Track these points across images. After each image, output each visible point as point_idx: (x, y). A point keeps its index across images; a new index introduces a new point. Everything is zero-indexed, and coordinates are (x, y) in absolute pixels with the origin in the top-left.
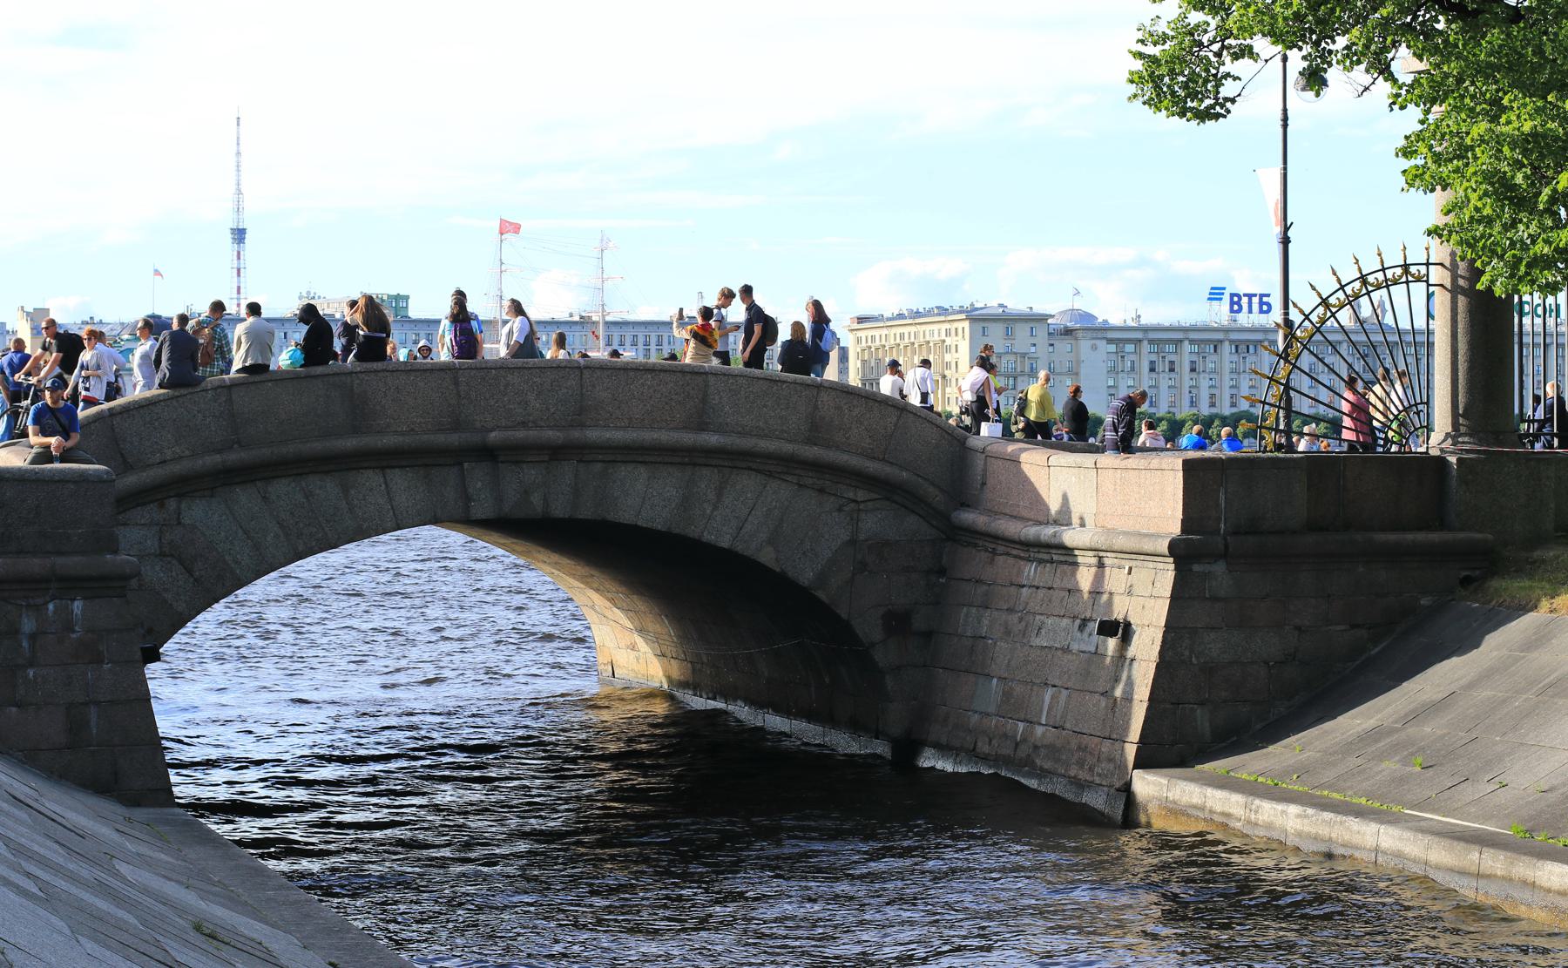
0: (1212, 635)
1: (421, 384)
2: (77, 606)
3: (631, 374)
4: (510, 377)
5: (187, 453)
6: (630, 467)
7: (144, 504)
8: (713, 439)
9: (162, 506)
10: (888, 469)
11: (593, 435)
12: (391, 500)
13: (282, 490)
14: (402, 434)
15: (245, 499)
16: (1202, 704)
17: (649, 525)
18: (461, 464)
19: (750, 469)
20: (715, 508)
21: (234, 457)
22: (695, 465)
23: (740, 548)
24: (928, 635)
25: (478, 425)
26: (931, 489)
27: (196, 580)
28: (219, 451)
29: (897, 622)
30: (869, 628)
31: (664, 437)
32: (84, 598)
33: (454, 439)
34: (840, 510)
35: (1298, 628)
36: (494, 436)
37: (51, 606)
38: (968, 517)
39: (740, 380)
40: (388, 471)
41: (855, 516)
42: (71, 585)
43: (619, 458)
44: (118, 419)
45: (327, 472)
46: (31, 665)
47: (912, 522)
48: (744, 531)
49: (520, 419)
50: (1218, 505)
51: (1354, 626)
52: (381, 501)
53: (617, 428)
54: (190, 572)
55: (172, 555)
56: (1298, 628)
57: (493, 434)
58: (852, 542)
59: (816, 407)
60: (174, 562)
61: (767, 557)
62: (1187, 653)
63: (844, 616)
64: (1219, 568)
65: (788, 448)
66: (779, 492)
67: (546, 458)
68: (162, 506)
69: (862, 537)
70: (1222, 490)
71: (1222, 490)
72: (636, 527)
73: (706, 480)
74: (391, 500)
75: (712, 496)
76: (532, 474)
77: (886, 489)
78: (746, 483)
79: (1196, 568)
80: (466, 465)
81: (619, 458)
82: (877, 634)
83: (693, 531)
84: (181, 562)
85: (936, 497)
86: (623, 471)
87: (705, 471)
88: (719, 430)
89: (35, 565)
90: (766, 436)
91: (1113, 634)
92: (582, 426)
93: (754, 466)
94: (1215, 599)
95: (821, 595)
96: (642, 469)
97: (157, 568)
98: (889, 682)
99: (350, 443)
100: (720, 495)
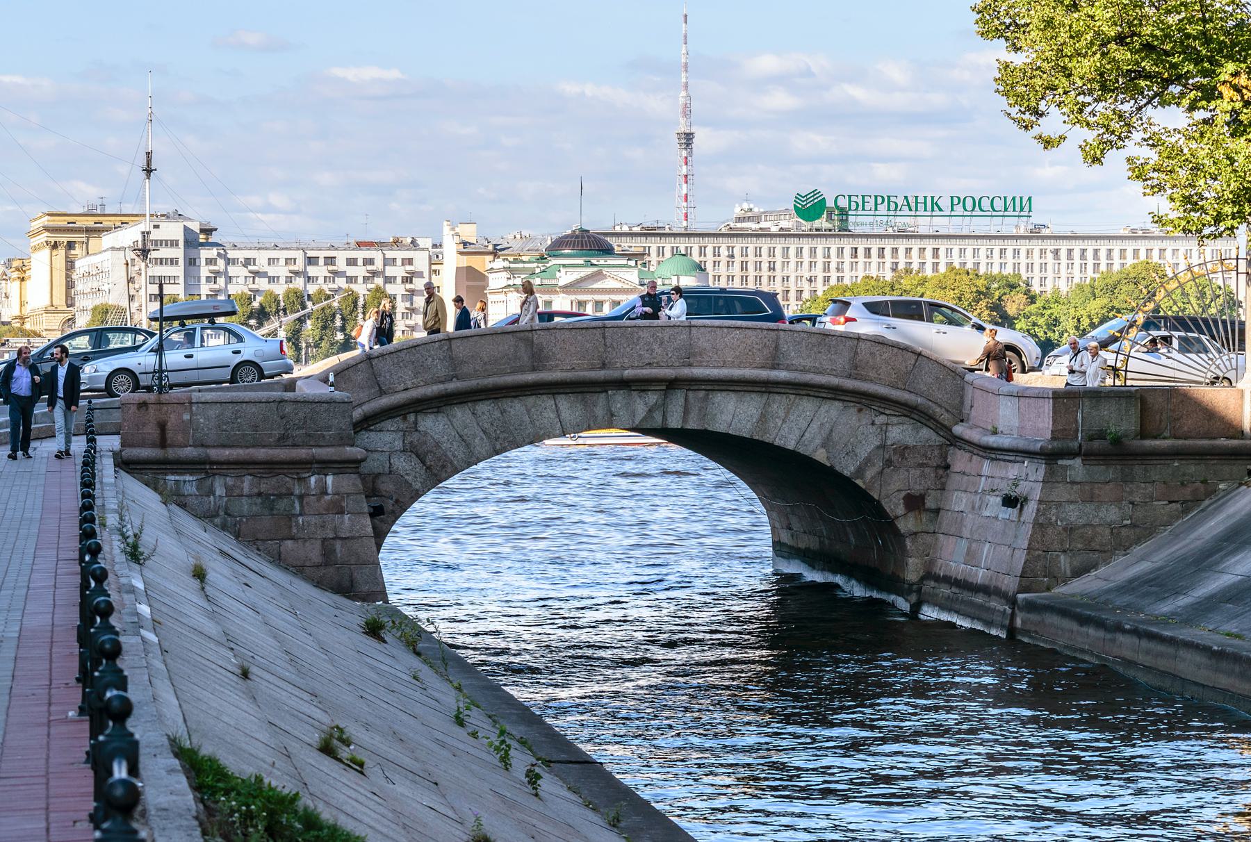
0: (1072, 507)
1: (580, 338)
2: (330, 479)
3: (725, 330)
4: (641, 333)
5: (422, 384)
6: (724, 394)
7: (394, 417)
8: (782, 375)
9: (405, 419)
10: (919, 400)
11: (698, 372)
12: (559, 416)
13: (484, 408)
14: (567, 370)
15: (461, 414)
16: (1064, 551)
17: (737, 434)
18: (607, 392)
19: (808, 395)
20: (784, 421)
21: (452, 386)
22: (770, 393)
23: (801, 450)
24: (937, 511)
25: (618, 365)
26: (938, 410)
27: (427, 468)
28: (443, 382)
29: (914, 502)
30: (894, 506)
31: (748, 373)
32: (334, 474)
33: (600, 374)
34: (873, 424)
35: (1132, 503)
36: (628, 373)
37: (313, 479)
38: (958, 429)
39: (802, 334)
40: (588, 396)
41: (884, 428)
42: (325, 466)
43: (717, 388)
44: (376, 360)
45: (515, 397)
46: (301, 514)
47: (925, 433)
48: (804, 438)
49: (647, 361)
50: (1077, 421)
51: (1170, 502)
52: (552, 416)
53: (714, 367)
54: (424, 463)
55: (411, 451)
56: (1132, 503)
57: (627, 372)
58: (882, 447)
59: (856, 353)
60: (414, 456)
61: (821, 456)
62: (1054, 518)
63: (876, 497)
64: (1078, 462)
65: (835, 381)
66: (831, 411)
67: (664, 388)
68: (405, 419)
69: (889, 442)
70: (1080, 411)
71: (1080, 411)
72: (727, 435)
73: (779, 404)
74: (559, 416)
75: (782, 414)
76: (652, 398)
77: (910, 411)
78: (807, 406)
79: (1060, 462)
80: (610, 392)
81: (717, 388)
82: (901, 510)
83: (768, 438)
84: (418, 456)
85: (945, 418)
86: (719, 397)
87: (777, 397)
88: (788, 368)
89: (302, 453)
90: (821, 373)
91: (1014, 506)
92: (690, 365)
93: (812, 393)
94: (1073, 483)
95: (859, 482)
96: (732, 395)
97: (402, 460)
98: (908, 543)
99: (531, 377)
100: (787, 413)
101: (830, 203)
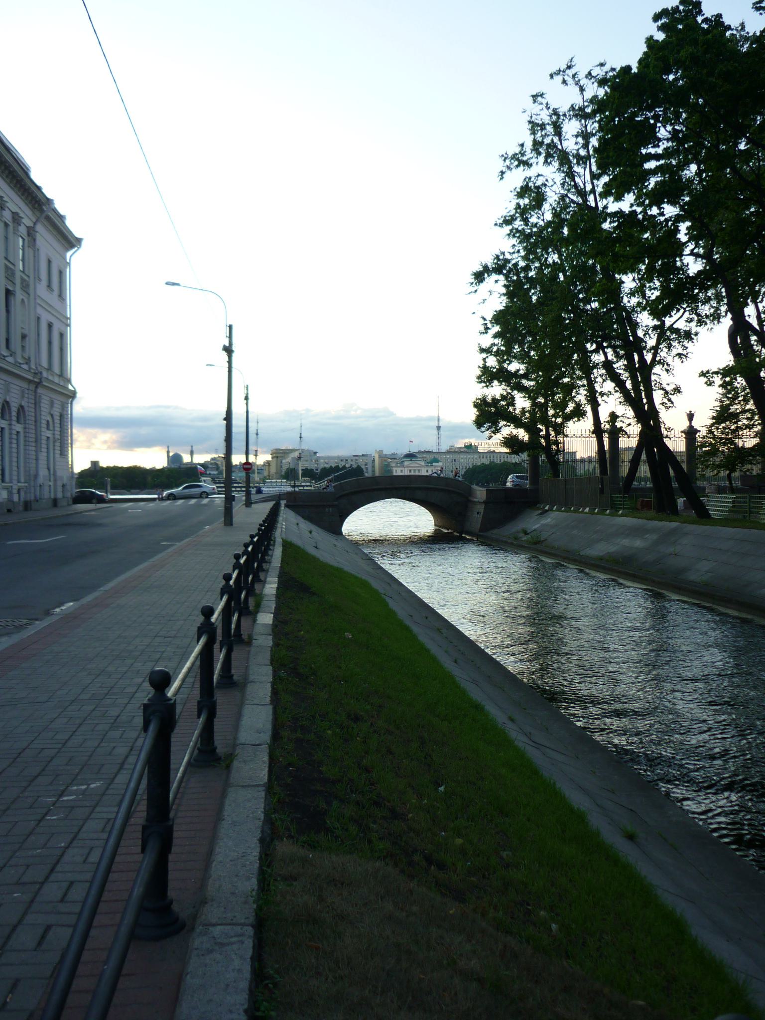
2: (331, 509)
101: (473, 445)
